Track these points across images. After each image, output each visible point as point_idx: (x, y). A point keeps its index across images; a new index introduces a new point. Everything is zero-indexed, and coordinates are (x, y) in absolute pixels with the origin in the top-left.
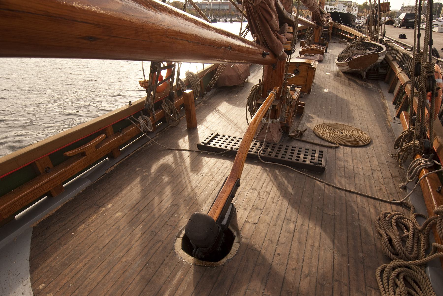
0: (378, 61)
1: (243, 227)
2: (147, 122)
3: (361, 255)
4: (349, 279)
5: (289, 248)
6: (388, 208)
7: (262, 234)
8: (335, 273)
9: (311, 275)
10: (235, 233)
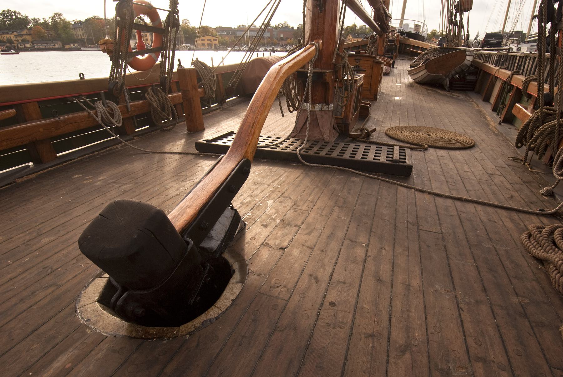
0: (466, 62)
1: (257, 254)
2: (112, 110)
3: (515, 300)
4: (506, 352)
5: (355, 291)
6: (532, 224)
7: (295, 266)
8: (470, 340)
9: (414, 349)
10: (236, 266)
